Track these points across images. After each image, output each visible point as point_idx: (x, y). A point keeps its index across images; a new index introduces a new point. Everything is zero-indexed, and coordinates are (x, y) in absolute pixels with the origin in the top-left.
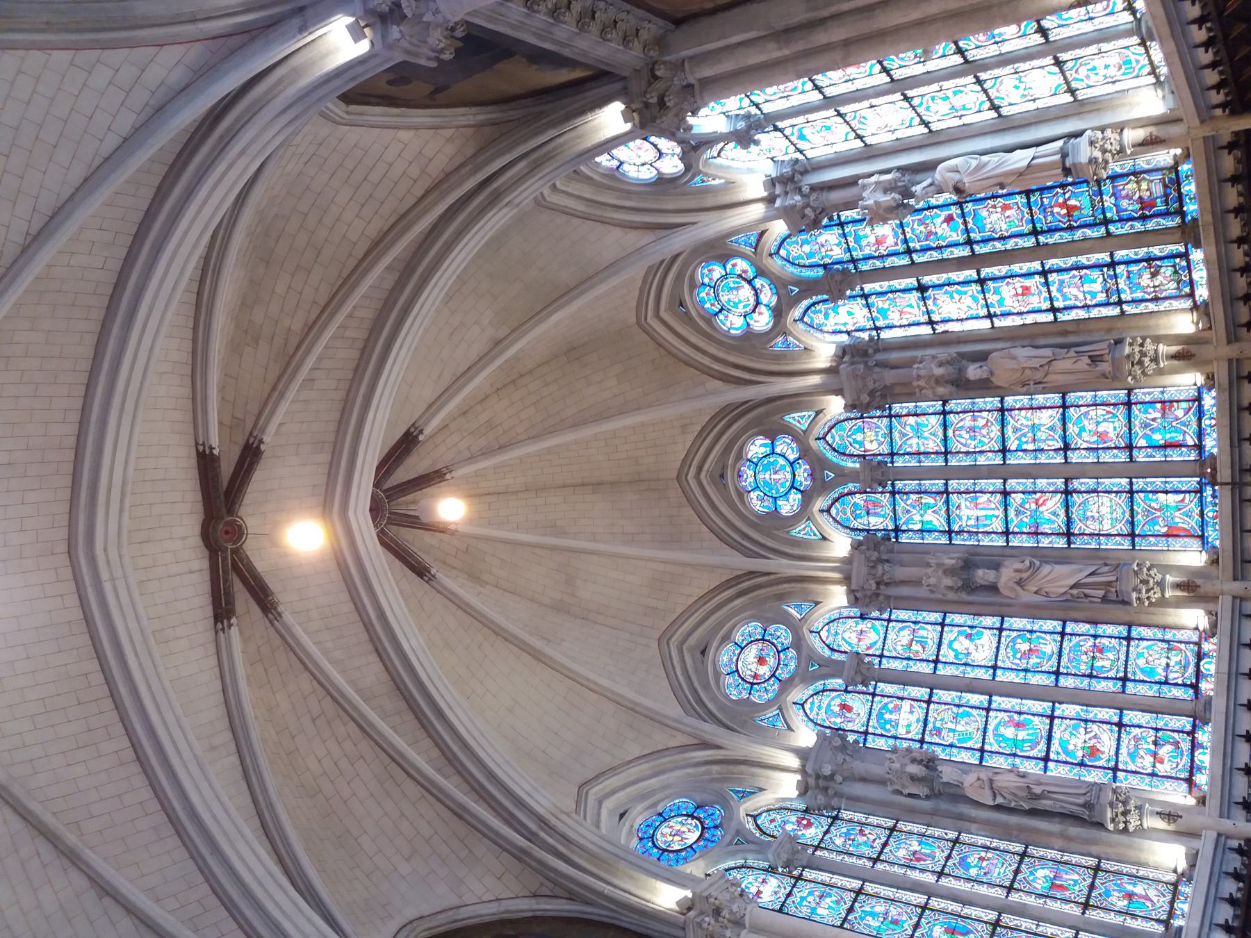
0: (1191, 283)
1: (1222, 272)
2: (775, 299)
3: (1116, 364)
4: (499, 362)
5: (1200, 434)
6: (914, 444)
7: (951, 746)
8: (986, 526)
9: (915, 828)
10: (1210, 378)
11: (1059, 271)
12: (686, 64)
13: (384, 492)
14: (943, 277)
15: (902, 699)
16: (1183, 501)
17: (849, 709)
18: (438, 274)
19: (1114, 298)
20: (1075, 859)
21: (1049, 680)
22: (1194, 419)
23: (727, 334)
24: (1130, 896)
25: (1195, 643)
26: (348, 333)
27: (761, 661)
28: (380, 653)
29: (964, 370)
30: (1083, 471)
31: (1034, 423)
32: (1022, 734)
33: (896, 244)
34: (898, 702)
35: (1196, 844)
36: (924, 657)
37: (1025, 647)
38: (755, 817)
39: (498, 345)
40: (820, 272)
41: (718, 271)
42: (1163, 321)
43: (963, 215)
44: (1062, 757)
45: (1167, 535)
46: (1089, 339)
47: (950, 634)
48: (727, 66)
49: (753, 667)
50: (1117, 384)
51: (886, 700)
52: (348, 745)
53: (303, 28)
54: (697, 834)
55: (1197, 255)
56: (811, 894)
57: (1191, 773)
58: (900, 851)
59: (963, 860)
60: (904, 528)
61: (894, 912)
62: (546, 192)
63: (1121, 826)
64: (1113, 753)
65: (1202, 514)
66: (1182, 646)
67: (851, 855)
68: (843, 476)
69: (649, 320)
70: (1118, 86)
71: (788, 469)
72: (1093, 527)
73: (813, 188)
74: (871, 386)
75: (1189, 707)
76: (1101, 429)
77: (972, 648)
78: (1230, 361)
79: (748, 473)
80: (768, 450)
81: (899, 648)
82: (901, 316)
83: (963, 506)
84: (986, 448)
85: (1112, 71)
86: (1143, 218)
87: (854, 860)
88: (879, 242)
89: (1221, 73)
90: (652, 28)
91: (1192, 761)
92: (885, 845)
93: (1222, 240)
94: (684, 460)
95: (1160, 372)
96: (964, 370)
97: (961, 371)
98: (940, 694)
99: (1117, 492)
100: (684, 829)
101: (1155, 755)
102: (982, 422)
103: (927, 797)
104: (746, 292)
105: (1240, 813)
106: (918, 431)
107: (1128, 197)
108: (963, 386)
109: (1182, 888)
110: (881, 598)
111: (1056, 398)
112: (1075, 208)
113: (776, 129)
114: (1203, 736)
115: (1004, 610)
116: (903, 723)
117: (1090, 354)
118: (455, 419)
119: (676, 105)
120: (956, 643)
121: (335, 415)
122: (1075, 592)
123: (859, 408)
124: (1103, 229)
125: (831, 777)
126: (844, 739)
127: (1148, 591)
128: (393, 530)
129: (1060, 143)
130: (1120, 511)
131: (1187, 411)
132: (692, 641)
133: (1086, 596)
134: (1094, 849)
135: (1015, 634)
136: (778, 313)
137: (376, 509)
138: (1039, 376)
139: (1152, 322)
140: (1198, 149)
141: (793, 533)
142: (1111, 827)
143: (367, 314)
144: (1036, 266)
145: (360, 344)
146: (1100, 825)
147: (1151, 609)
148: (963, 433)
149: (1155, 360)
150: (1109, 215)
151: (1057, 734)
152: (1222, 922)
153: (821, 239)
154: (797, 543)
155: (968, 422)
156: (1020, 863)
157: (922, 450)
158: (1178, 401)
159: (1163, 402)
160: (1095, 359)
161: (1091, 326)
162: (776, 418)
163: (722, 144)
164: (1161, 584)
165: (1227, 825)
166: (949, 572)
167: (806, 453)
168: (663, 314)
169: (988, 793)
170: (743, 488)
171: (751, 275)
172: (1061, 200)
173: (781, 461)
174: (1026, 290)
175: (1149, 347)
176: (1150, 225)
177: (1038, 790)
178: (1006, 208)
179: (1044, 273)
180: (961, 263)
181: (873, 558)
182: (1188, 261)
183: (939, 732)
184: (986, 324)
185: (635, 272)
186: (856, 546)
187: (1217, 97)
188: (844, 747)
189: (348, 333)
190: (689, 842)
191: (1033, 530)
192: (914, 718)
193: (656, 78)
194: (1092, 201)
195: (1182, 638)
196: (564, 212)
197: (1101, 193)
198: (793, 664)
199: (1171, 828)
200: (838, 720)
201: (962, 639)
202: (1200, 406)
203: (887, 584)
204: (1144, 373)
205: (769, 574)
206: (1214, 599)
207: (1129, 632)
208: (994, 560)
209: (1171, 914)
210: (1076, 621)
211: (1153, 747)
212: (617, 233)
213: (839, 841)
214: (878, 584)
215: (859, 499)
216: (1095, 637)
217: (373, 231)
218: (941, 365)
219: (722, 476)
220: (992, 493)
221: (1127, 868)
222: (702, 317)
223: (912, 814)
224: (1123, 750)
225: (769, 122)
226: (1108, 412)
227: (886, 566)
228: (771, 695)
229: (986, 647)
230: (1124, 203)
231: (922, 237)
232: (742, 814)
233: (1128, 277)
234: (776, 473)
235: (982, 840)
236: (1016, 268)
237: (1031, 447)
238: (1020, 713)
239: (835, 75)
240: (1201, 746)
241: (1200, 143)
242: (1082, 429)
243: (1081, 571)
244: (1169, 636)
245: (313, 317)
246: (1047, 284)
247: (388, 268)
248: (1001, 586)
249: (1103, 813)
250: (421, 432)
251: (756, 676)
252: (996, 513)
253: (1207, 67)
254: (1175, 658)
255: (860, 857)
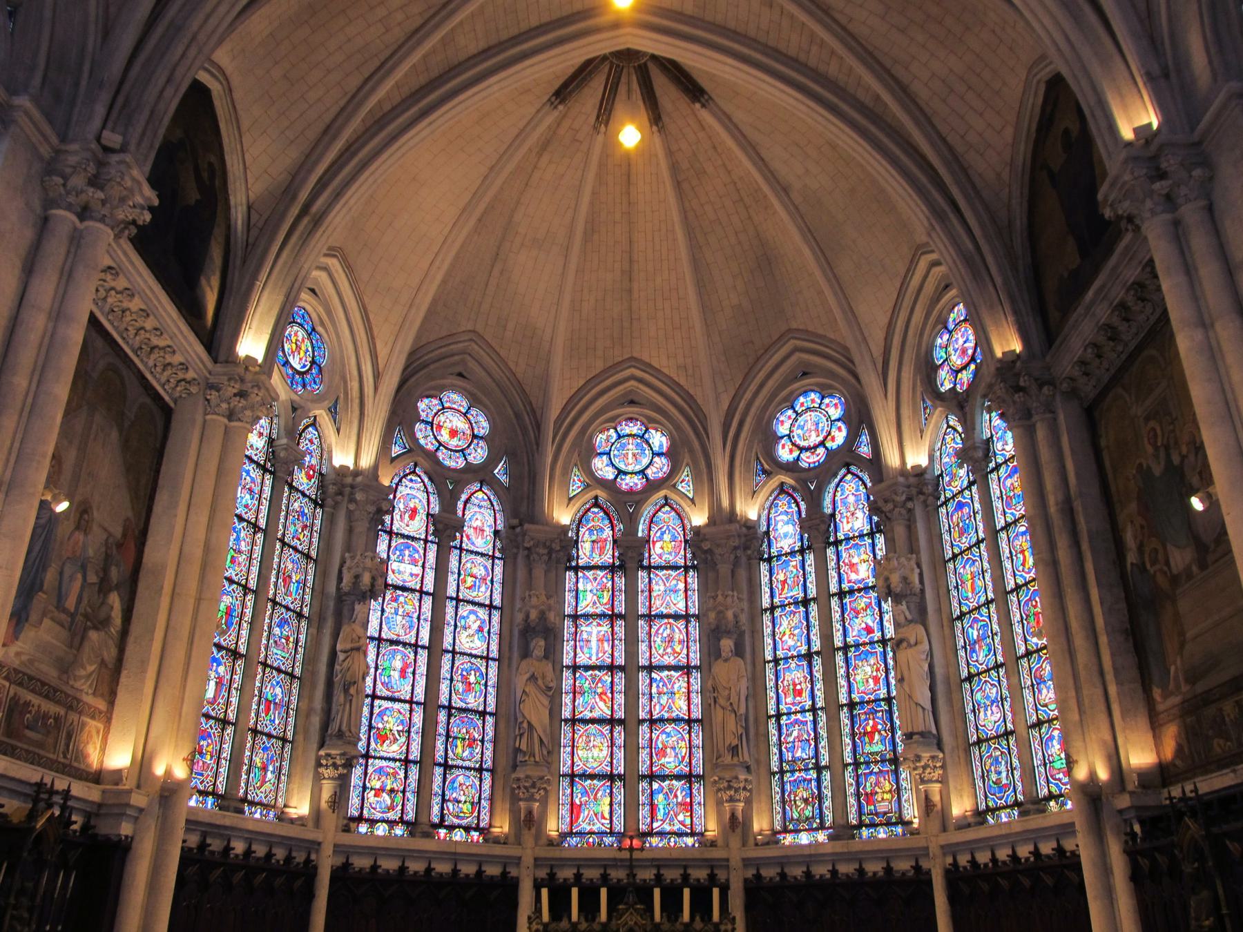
0: (797, 831)
1: (809, 857)
2: (804, 465)
3: (731, 767)
4: (766, 189)
5: (661, 834)
6: (658, 588)
7: (383, 611)
8: (581, 648)
9: (310, 578)
10: (713, 844)
11: (815, 722)
12: (1049, 416)
13: (645, 64)
14: (814, 621)
15: (423, 566)
16: (603, 817)
17: (412, 517)
18: (869, 148)
19: (786, 767)
20: (291, 720)
21: (444, 700)
22: (675, 828)
23: (773, 417)
24: (264, 768)
25: (478, 824)
26: (815, 49)
27: (453, 433)
28: (486, 53)
29: (729, 633)
30: (631, 653)
31: (676, 696)
32: (396, 675)
33: (849, 582)
34: (420, 563)
35: (310, 824)
36: (461, 588)
37: (472, 679)
38: (314, 424)
39: (784, 190)
40: (828, 511)
41: (835, 413)
42: (764, 806)
43: (872, 643)
44: (376, 710)
45: (572, 804)
46: (752, 744)
47: (482, 613)
48: (1045, 454)
49: (448, 425)
50: (708, 767)
51: (422, 552)
52: (399, 16)
53: (1150, 78)
54: (298, 367)
55: (822, 837)
56: (253, 481)
57: (367, 820)
58: (290, 562)
59: (286, 621)
60: (580, 574)
61: (242, 558)
62: (934, 256)
63: (324, 762)
64: (383, 754)
65: (591, 833)
66: (476, 814)
67: (286, 518)
68: (632, 521)
69: (792, 341)
70: (979, 783)
71: (638, 468)
72: (581, 743)
73: (910, 511)
74: (718, 551)
75: (423, 819)
76: (668, 750)
77: (471, 632)
78: (727, 860)
79: (634, 428)
80: (656, 449)
81: (469, 565)
82: (784, 580)
83: (599, 628)
84: (653, 651)
85: (994, 777)
86: (858, 795)
87: (282, 520)
88: (852, 566)
89: (986, 865)
90: (1089, 389)
91: (377, 821)
92: (295, 549)
93: (836, 858)
94: (650, 366)
95: (719, 803)
96: (729, 633)
97: (728, 633)
98: (428, 602)
99: (612, 763)
100: (302, 354)
101: (382, 789)
102: (678, 649)
103: (338, 589)
104: (814, 439)
105: (339, 861)
106: (671, 592)
107: (877, 783)
108: (712, 637)
109: (210, 800)
110: (515, 550)
111: (697, 713)
112: (872, 739)
113: (971, 484)
114: (399, 831)
115: (506, 662)
116: (402, 567)
117: (736, 741)
118: (710, 138)
119: (1014, 402)
120: (473, 618)
121: (732, 24)
122: (525, 725)
123: (696, 541)
124: (850, 761)
125: (352, 500)
126: (387, 512)
127: (525, 788)
128: (605, 68)
129: (934, 731)
130: (595, 765)
131: (682, 823)
132: (472, 364)
133: (521, 735)
134: (300, 738)
135: (484, 670)
136: (792, 467)
137: (628, 55)
138: (722, 701)
139: (764, 798)
140: (918, 842)
141: (575, 469)
142: (322, 753)
143: (833, 70)
144: (820, 704)
145: (802, 57)
146: (322, 745)
147: (508, 790)
148: (668, 631)
149: (731, 800)
150: (863, 767)
151: (397, 706)
152: (433, 866)
153: (859, 514)
154: (566, 473)
155: (677, 636)
156: (286, 673)
157: (654, 594)
158: (691, 816)
159: (691, 804)
160: (734, 750)
161: (763, 746)
162: (687, 459)
163: (960, 429)
164: (531, 799)
165: (327, 850)
166: (542, 616)
167: (652, 486)
168: (798, 355)
169: (349, 646)
170: (620, 423)
171: (829, 444)
172: (880, 727)
173: (645, 461)
174: (799, 693)
175: (743, 794)
176: (852, 801)
177: (352, 691)
178: (876, 680)
179: (813, 709)
180: (827, 637)
181: (554, 546)
182: (817, 829)
183: (395, 600)
184: (769, 657)
185: (844, 334)
186: (565, 529)
187: (963, 860)
188: (380, 512)
189: (815, 49)
190: (291, 359)
191: (578, 689)
192: (407, 577)
193: (1041, 386)
194: (877, 753)
195: (482, 814)
196: (908, 270)
197: (883, 761)
198: (452, 464)
199: (324, 805)
200: (402, 506)
201: (478, 623)
202: (687, 835)
203: (528, 557)
204: (719, 790)
205: (538, 445)
206: (519, 842)
207: (487, 770)
208: (552, 652)
209: (252, 803)
210: (496, 725)
211: (388, 788)
212: (883, 320)
213: (296, 505)
214: (528, 549)
215: (608, 533)
216: (482, 741)
217: (917, 88)
218: (735, 616)
219: (632, 402)
220: (612, 655)
221: (286, 764)
222: (792, 393)
223: (322, 575)
224: (384, 763)
225: (980, 477)
226: (683, 758)
227: (546, 558)
228: (422, 442)
229: (472, 645)
230: (873, 779)
231: (853, 605)
232: (317, 412)
233: (805, 780)
234: (634, 455)
235: (302, 637)
236: (819, 685)
237: (654, 690)
238: (414, 673)
239: (1023, 542)
240: (391, 828)
241: (923, 844)
242: (668, 735)
243: (544, 731)
244: (485, 803)
245: (838, 16)
246: (803, 711)
247: (877, 98)
248: (528, 660)
249: (334, 747)
250: (703, 106)
251: (440, 427)
252: (594, 658)
253: (993, 854)
254: (466, 808)
255: (285, 527)
